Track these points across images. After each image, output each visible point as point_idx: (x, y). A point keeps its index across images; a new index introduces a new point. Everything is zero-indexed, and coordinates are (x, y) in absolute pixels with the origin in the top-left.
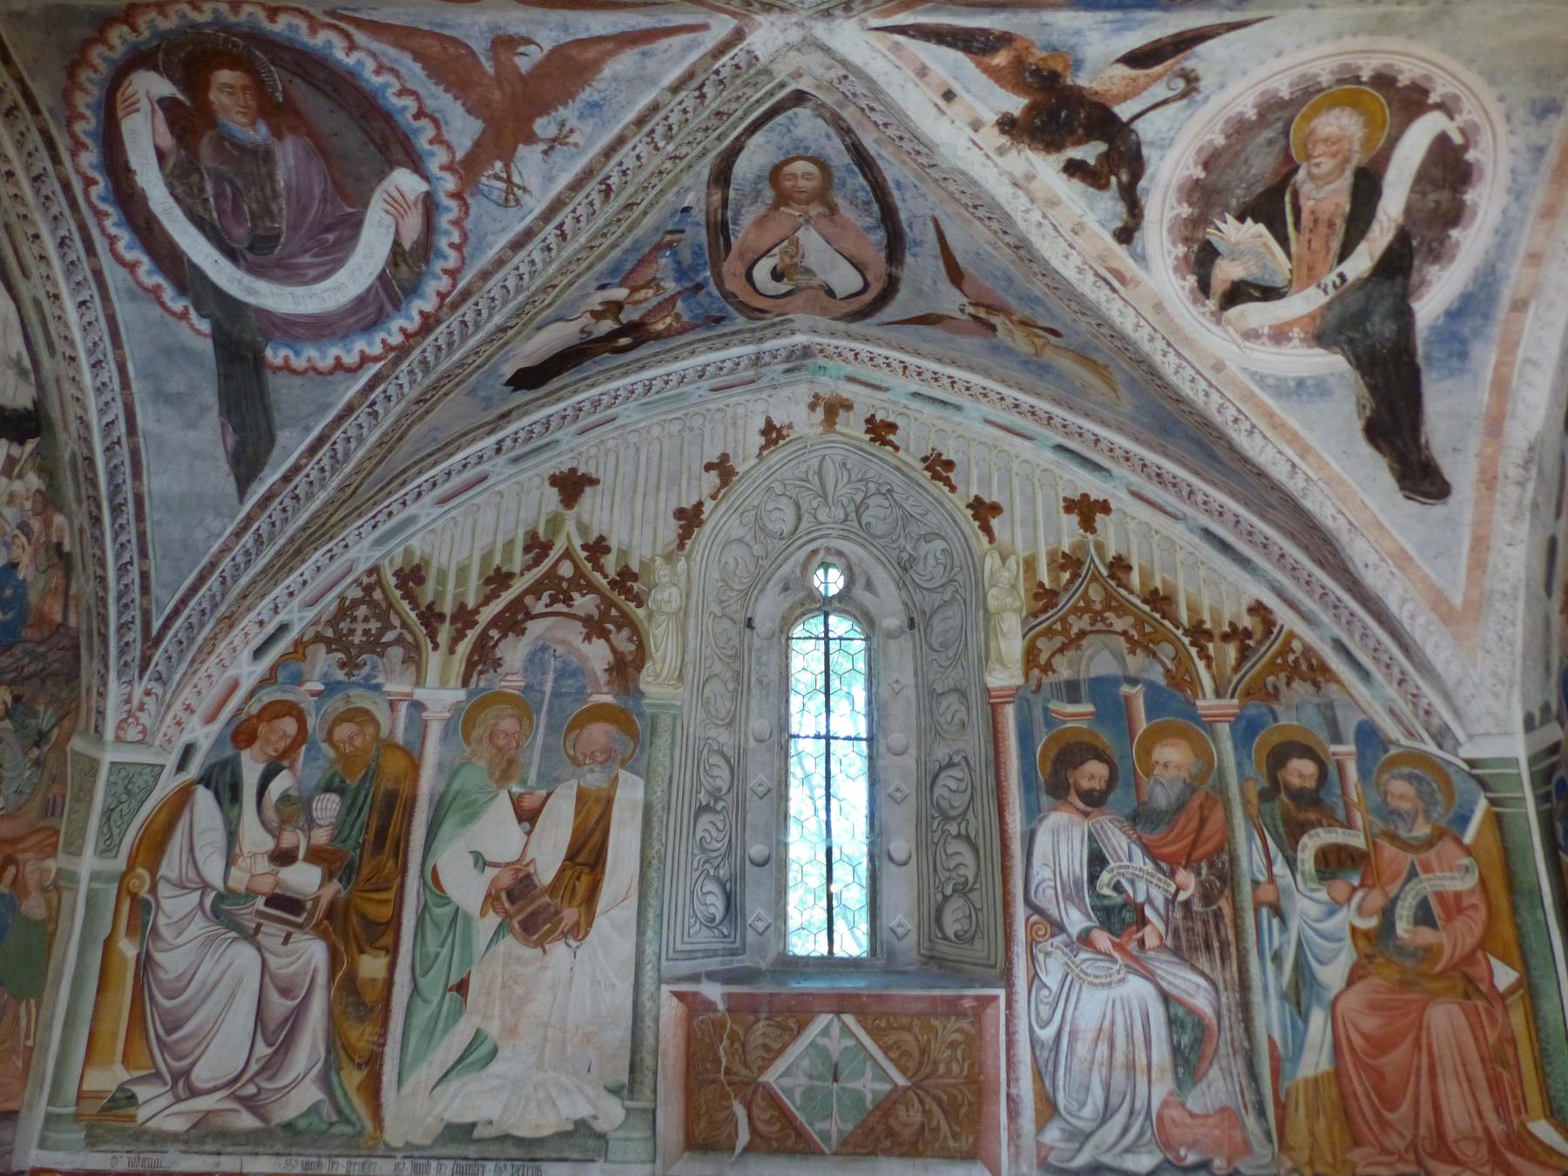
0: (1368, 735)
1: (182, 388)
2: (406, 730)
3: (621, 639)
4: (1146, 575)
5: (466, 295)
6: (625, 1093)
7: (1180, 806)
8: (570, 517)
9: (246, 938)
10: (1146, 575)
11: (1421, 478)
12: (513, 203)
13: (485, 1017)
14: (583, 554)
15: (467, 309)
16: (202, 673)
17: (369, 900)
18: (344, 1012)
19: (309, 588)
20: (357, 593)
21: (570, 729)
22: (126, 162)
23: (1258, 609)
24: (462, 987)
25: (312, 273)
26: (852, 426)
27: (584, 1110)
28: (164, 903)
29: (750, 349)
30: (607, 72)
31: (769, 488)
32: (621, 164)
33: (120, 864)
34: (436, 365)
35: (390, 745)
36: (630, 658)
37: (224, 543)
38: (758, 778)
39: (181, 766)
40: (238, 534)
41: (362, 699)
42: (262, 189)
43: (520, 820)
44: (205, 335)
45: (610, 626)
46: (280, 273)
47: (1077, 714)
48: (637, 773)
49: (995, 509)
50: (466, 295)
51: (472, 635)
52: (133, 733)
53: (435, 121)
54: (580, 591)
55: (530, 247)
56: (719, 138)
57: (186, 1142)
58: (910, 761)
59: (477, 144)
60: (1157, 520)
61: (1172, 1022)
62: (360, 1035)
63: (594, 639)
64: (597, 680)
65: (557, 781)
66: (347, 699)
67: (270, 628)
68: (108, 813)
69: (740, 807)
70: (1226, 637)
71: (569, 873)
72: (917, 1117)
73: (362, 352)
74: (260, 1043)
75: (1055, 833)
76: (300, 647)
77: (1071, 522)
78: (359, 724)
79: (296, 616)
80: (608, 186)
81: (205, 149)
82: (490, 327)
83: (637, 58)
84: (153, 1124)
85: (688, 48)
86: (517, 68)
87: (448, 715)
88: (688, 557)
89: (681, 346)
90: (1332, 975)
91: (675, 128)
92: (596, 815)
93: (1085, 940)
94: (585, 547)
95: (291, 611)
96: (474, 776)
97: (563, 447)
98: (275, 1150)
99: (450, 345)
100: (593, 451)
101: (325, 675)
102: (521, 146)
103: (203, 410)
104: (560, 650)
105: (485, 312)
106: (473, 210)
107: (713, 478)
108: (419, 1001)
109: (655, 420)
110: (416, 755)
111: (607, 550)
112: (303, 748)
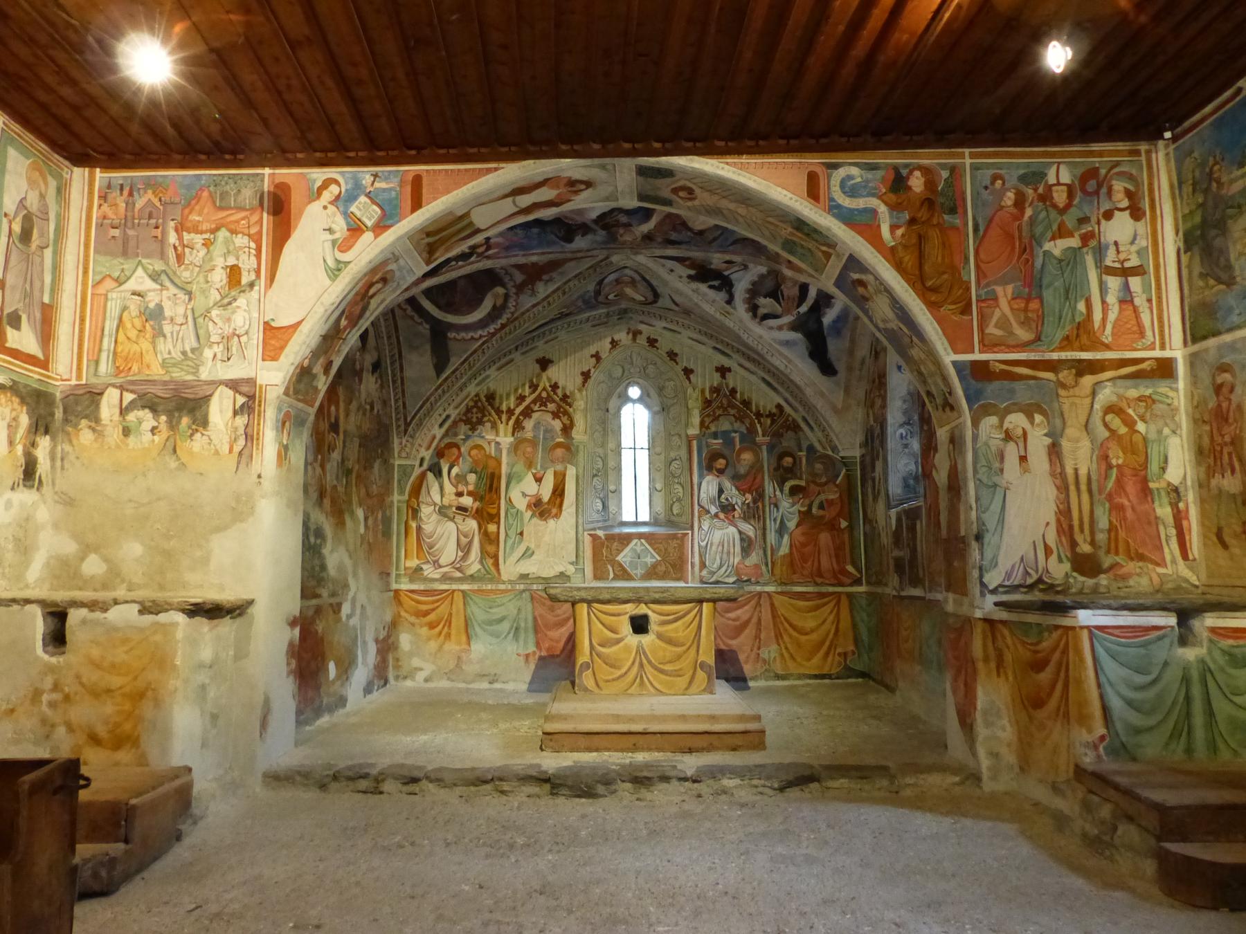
0: (811, 449)
4: (742, 394)
5: (516, 319)
7: (748, 474)
10: (742, 394)
11: (827, 368)
15: (517, 323)
20: (471, 404)
23: (779, 406)
24: (521, 534)
26: (642, 340)
27: (562, 569)
29: (605, 310)
33: (406, 497)
35: (490, 457)
38: (611, 464)
39: (421, 465)
40: (436, 390)
41: (480, 442)
47: (717, 443)
49: (692, 371)
50: (516, 319)
51: (514, 418)
52: (404, 455)
58: (662, 457)
60: (746, 374)
61: (742, 540)
62: (491, 549)
68: (399, 481)
69: (606, 475)
70: (767, 416)
72: (663, 568)
75: (220, 397)
76: (455, 423)
77: (717, 376)
90: (791, 525)
93: (716, 515)
96: (519, 467)
107: (594, 360)
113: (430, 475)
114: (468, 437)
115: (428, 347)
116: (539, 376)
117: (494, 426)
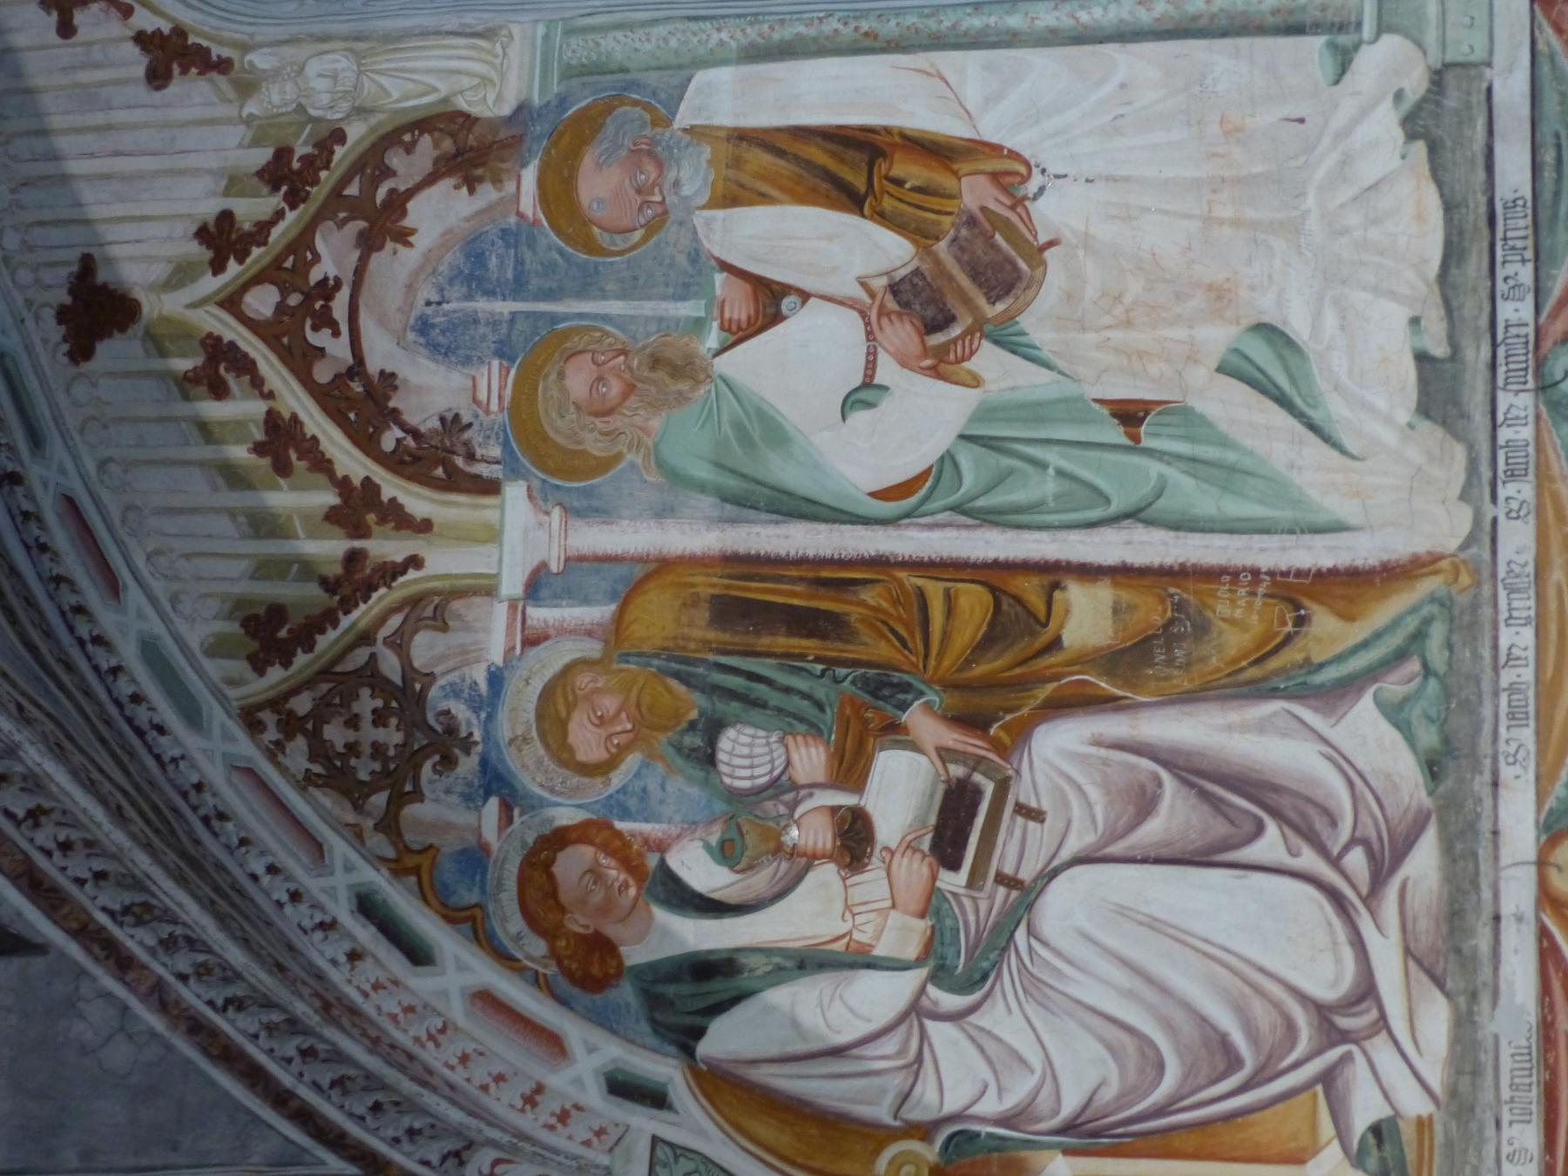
2: (586, 601)
3: (406, 167)
6: (1343, 39)
8: (158, 306)
9: (1030, 907)
13: (1192, 358)
14: (233, 268)
16: (458, 1077)
17: (946, 636)
18: (1187, 666)
19: (289, 863)
20: (297, 754)
21: (592, 247)
24: (1130, 415)
27: (1385, 124)
28: (951, 1105)
36: (448, 145)
37: (144, 998)
39: (655, 1098)
40: (122, 963)
43: (777, 318)
45: (381, 194)
48: (684, 87)
51: (392, 487)
54: (310, 265)
57: (1473, 996)
62: (1237, 624)
63: (408, 222)
64: (490, 208)
65: (695, 256)
66: (519, 741)
67: (365, 934)
71: (888, 204)
74: (1262, 850)
76: (409, 863)
78: (571, 708)
79: (341, 882)
84: (1436, 1081)
87: (556, 513)
88: (245, 48)
92: (766, 158)
94: (218, 267)
95: (332, 892)
96: (686, 435)
98: (1486, 792)
100: (24, 276)
101: (467, 798)
104: (427, 292)
108: (1161, 503)
110: (639, 571)
111: (226, 217)
112: (619, 825)
113: (726, 1039)
114: (495, 782)
116: (157, 343)
117: (434, 609)
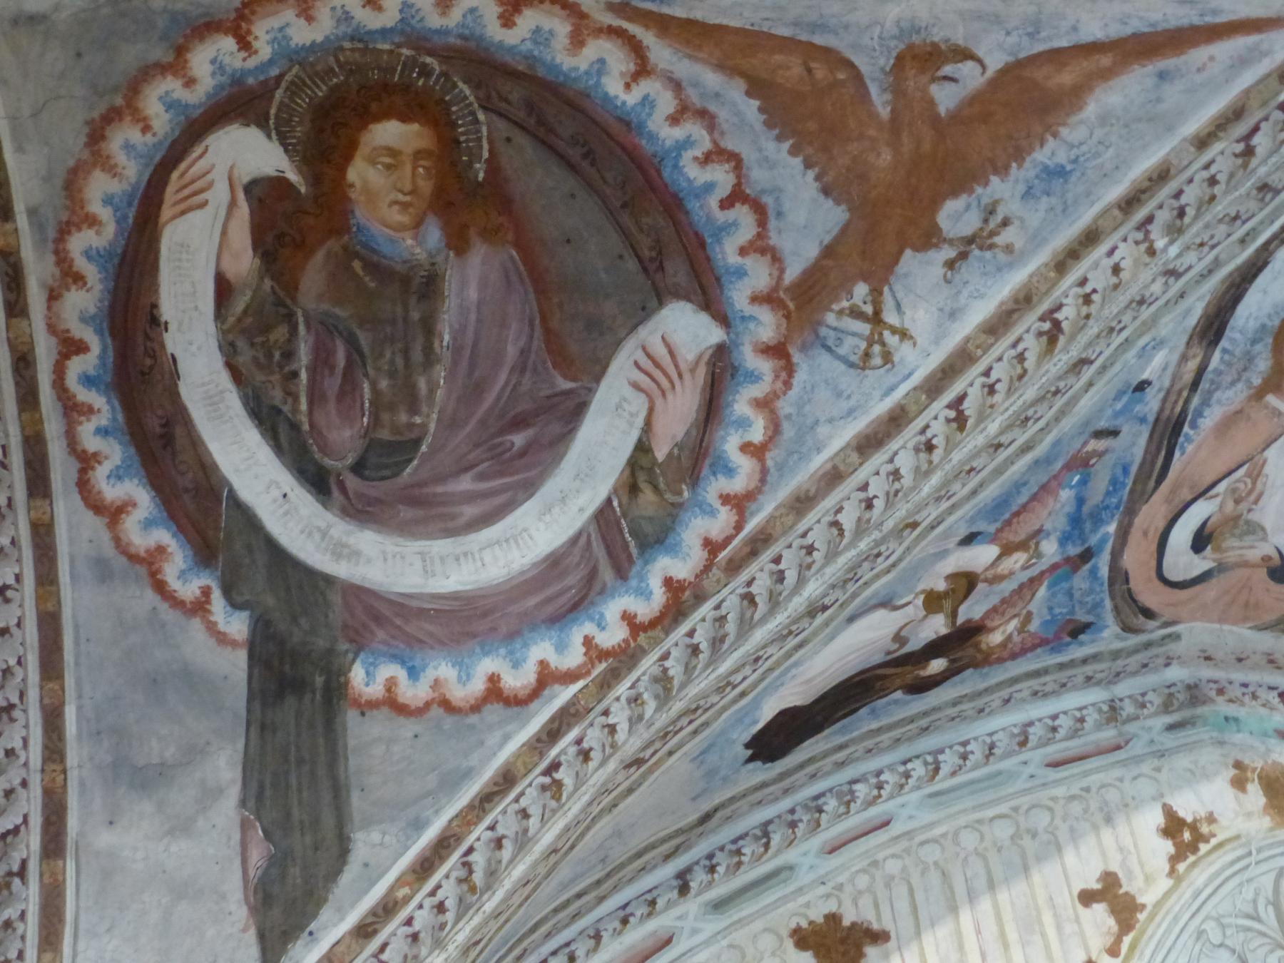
1: (170, 753)
12: (877, 361)
15: (759, 573)
22: (155, 306)
25: (470, 511)
29: (1095, 696)
30: (1091, 109)
31: (1200, 933)
32: (1083, 282)
34: (683, 686)
42: (406, 352)
44: (234, 644)
46: (406, 513)
53: (760, 210)
55: (894, 445)
56: (1243, 241)
59: (829, 252)
73: (543, 664)
80: (1057, 325)
81: (313, 278)
82: (798, 604)
83: (1150, 82)
85: (1243, 62)
86: (932, 103)
89: (1015, 680)
91: (1190, 212)
97: (804, 878)
99: (717, 642)
100: (862, 881)
102: (908, 253)
103: (210, 794)
105: (791, 576)
106: (800, 377)
107: (1100, 917)
109: (962, 821)
115: (225, 766)
